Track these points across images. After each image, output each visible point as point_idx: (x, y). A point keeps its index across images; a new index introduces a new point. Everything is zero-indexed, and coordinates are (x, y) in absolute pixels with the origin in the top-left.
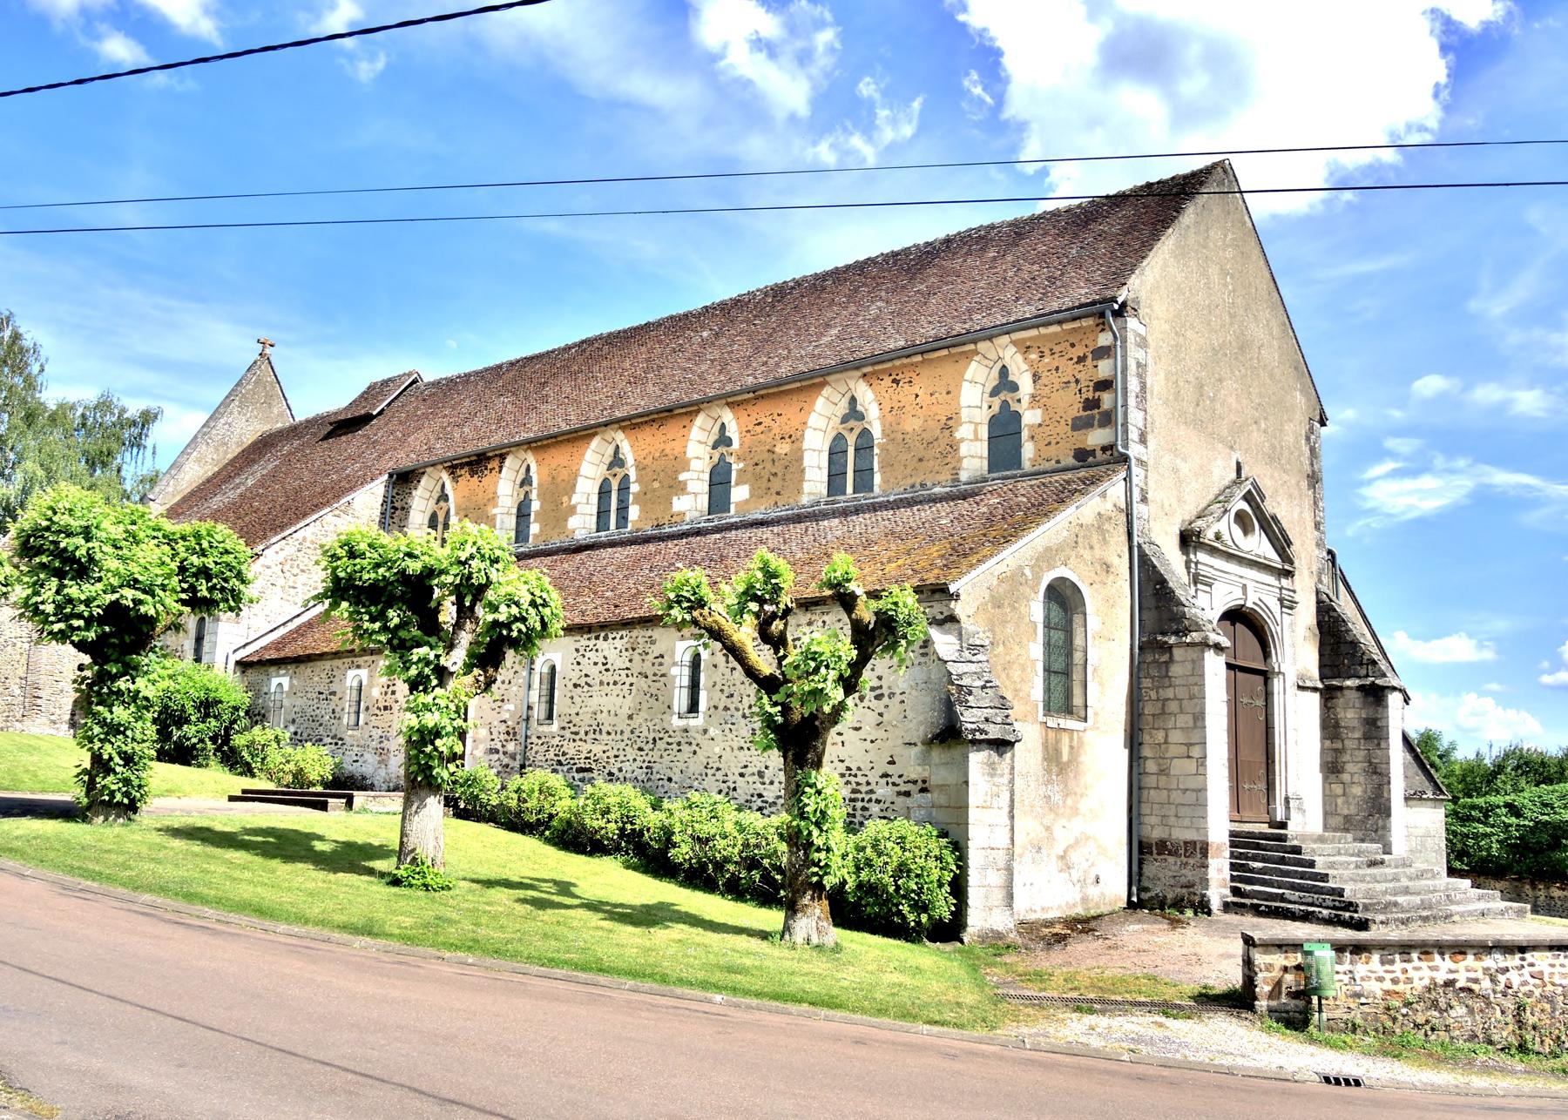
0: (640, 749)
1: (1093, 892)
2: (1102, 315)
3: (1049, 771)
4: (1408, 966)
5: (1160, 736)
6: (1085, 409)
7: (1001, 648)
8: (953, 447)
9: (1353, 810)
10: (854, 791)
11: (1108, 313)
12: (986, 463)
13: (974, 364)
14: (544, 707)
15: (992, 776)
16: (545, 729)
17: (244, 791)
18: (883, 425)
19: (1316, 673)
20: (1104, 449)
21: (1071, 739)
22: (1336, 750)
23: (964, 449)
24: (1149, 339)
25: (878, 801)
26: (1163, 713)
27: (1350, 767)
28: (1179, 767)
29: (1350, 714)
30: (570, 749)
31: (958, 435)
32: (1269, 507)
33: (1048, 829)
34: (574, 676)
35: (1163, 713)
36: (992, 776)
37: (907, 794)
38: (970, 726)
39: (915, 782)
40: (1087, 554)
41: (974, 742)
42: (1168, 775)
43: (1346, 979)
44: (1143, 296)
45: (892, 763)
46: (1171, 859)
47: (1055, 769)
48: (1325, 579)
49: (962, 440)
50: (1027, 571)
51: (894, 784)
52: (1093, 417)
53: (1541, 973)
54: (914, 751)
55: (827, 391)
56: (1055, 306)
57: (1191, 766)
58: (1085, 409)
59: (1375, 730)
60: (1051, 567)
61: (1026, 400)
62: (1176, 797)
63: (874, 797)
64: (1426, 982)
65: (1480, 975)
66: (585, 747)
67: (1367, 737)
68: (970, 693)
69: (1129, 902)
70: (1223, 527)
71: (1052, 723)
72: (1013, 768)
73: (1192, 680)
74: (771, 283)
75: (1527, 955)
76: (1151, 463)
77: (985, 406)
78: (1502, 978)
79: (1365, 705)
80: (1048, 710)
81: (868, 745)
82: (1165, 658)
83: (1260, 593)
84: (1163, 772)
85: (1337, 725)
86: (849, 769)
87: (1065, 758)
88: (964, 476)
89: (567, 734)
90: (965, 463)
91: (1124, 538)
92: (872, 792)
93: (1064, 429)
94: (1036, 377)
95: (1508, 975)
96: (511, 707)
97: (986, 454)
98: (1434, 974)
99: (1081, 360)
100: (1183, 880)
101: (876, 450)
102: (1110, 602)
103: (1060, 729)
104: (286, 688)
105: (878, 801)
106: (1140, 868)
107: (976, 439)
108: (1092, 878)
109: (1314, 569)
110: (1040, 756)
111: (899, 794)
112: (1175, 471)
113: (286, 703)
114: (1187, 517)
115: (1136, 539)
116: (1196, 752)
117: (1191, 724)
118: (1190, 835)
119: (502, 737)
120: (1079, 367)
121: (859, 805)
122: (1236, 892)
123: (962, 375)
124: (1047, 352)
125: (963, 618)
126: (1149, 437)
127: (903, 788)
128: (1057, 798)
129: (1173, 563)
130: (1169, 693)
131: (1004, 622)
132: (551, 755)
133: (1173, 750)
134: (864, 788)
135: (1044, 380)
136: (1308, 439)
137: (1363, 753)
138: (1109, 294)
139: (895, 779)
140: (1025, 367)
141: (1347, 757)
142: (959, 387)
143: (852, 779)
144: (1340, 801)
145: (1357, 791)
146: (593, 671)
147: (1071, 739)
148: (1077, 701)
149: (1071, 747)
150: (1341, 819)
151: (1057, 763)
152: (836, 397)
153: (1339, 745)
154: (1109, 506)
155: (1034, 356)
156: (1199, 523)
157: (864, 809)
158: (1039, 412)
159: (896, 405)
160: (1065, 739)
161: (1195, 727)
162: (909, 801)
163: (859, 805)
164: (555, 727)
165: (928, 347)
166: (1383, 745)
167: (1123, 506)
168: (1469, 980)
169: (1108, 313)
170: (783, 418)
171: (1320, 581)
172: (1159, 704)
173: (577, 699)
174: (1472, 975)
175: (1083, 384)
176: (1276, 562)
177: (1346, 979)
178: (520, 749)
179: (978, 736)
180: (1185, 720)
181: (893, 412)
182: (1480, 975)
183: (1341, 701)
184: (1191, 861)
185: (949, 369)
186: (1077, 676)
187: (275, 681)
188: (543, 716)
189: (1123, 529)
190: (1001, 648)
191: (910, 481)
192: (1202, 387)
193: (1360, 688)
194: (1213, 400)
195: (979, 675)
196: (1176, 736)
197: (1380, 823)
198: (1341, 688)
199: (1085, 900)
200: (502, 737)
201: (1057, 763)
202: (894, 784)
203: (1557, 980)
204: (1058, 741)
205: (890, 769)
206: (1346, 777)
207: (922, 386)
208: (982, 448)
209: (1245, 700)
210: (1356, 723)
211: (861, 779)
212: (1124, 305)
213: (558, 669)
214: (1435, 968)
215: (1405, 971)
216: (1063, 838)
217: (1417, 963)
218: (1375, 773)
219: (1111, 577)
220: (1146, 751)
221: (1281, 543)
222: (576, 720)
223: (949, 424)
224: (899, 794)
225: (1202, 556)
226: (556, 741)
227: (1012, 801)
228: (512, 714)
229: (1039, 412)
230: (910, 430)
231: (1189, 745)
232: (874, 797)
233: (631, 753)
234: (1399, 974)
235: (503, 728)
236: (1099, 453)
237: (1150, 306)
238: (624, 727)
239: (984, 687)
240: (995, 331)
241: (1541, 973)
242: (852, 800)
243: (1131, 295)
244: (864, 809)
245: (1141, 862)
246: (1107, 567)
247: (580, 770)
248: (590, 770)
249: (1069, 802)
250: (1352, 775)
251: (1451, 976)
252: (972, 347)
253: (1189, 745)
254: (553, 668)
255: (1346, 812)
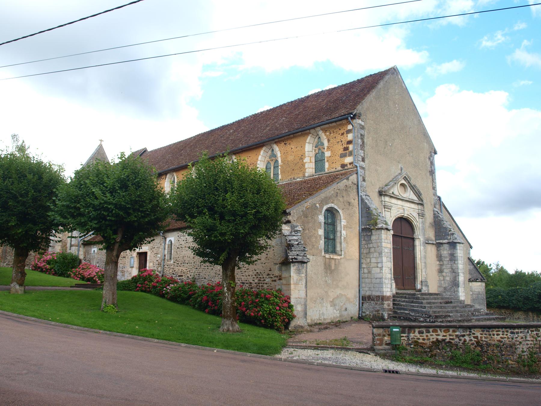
0: (196, 268)
1: (345, 313)
2: (347, 119)
3: (326, 273)
4: (428, 334)
5: (368, 260)
6: (344, 150)
7: (307, 231)
8: (303, 165)
9: (447, 285)
10: (259, 280)
11: (349, 118)
12: (314, 170)
13: (309, 137)
14: (169, 255)
15: (299, 273)
16: (169, 263)
17: (76, 285)
18: (281, 159)
19: (434, 239)
20: (350, 164)
21: (335, 262)
22: (441, 265)
23: (306, 166)
24: (366, 127)
25: (266, 283)
26: (369, 252)
27: (445, 271)
28: (375, 270)
29: (445, 252)
30: (176, 269)
31: (305, 161)
32: (412, 182)
33: (326, 292)
34: (177, 245)
35: (369, 252)
36: (299, 273)
37: (275, 281)
38: (290, 257)
39: (277, 277)
40: (341, 199)
41: (293, 262)
42: (371, 273)
43: (406, 339)
44: (362, 112)
45: (270, 270)
46: (372, 302)
47: (329, 272)
48: (438, 206)
49: (306, 163)
50: (318, 205)
51: (271, 278)
52: (346, 153)
53: (477, 337)
54: (278, 266)
55: (264, 148)
56: (333, 116)
57: (378, 270)
58: (344, 150)
59: (453, 258)
60: (327, 204)
61: (326, 148)
62: (374, 281)
63: (265, 282)
64: (435, 340)
65: (454, 337)
66: (181, 268)
67: (451, 260)
68: (293, 246)
69: (359, 317)
70: (396, 190)
71: (327, 256)
72: (306, 271)
73: (378, 241)
74: (254, 114)
75: (472, 331)
76: (367, 168)
77: (314, 151)
78: (462, 338)
79: (450, 249)
80: (326, 251)
81: (264, 265)
82: (369, 234)
83: (410, 211)
84: (369, 272)
85: (441, 256)
86: (257, 273)
87: (333, 268)
88: (307, 175)
89: (175, 264)
90: (307, 170)
91: (356, 193)
92: (264, 280)
93: (338, 158)
94: (329, 141)
95: (465, 337)
96: (159, 256)
97: (314, 167)
98: (438, 337)
99: (343, 134)
100: (376, 309)
101: (280, 167)
102: (350, 216)
103: (330, 258)
104: (96, 252)
105: (266, 283)
106: (362, 305)
107: (311, 162)
108: (344, 309)
109: (433, 203)
110: (323, 268)
111: (273, 281)
112: (376, 170)
113: (96, 257)
114: (381, 186)
115: (360, 194)
116: (380, 265)
117: (378, 256)
118: (378, 294)
119: (157, 266)
120: (342, 137)
121: (261, 285)
122: (395, 312)
123: (306, 140)
124: (332, 132)
125: (292, 221)
126: (366, 160)
127: (274, 279)
128: (330, 281)
129: (374, 203)
130: (371, 245)
131: (308, 222)
132: (171, 271)
133: (373, 265)
134: (262, 279)
135: (331, 141)
136: (429, 159)
137: (449, 266)
138: (351, 112)
139: (272, 276)
140: (325, 137)
141: (444, 267)
142: (305, 145)
143: (259, 276)
144: (442, 282)
145: (448, 278)
146: (183, 243)
147: (335, 262)
148: (338, 249)
149: (335, 264)
150: (443, 289)
151: (329, 269)
152: (267, 150)
153: (442, 263)
154: (350, 183)
155: (328, 134)
156: (386, 188)
157: (262, 286)
158: (330, 152)
159: (285, 152)
160: (333, 262)
161: (379, 257)
162: (275, 283)
163: (261, 285)
164: (172, 262)
165: (295, 132)
166: (456, 263)
167: (356, 183)
168: (450, 339)
169: (349, 118)
170: (251, 158)
171: (435, 207)
172: (368, 250)
173: (178, 252)
174: (451, 337)
175: (343, 142)
176: (415, 198)
177: (406, 339)
178: (162, 269)
179: (294, 260)
180: (376, 255)
181: (284, 154)
182: (454, 337)
183: (442, 248)
184: (379, 303)
185: (301, 139)
186: (338, 240)
187: (93, 250)
188: (169, 258)
189: (355, 190)
190: (307, 231)
191: (290, 177)
192: (387, 142)
193: (448, 243)
194: (391, 146)
195: (297, 240)
196: (373, 260)
197: (456, 289)
198: (442, 244)
199: (341, 316)
200: (157, 266)
201: (329, 269)
202: (271, 278)
203: (483, 339)
204: (330, 262)
205: (270, 273)
206: (444, 274)
207: (293, 146)
208: (313, 165)
209: (406, 248)
210: (447, 255)
211: (261, 276)
212: (355, 115)
213: (173, 243)
214: (438, 335)
215: (427, 336)
216: (332, 294)
217: (432, 333)
218: (454, 272)
219: (351, 207)
220: (364, 266)
221: (418, 194)
222: (178, 259)
223: (302, 157)
224: (273, 281)
225: (387, 199)
226: (172, 267)
227: (306, 282)
228: (160, 258)
229: (330, 152)
230: (290, 160)
231: (377, 263)
232: (265, 282)
233: (194, 270)
234: (425, 337)
235: (157, 263)
236: (348, 165)
237: (366, 115)
238: (191, 261)
239: (298, 244)
240: (315, 126)
241: (477, 337)
242: (259, 283)
243: (358, 112)
244: (262, 286)
245: (362, 303)
246: (349, 203)
247: (179, 276)
248: (182, 276)
249: (335, 283)
250: (446, 273)
251: (444, 338)
252: (308, 131)
253: (377, 263)
254: (171, 242)
255: (444, 286)
